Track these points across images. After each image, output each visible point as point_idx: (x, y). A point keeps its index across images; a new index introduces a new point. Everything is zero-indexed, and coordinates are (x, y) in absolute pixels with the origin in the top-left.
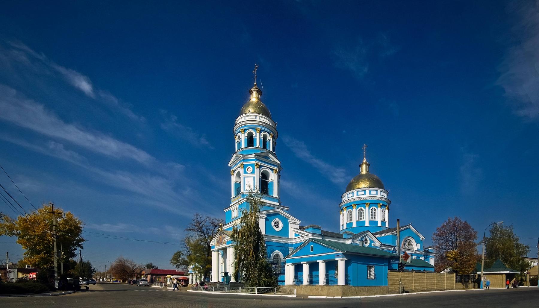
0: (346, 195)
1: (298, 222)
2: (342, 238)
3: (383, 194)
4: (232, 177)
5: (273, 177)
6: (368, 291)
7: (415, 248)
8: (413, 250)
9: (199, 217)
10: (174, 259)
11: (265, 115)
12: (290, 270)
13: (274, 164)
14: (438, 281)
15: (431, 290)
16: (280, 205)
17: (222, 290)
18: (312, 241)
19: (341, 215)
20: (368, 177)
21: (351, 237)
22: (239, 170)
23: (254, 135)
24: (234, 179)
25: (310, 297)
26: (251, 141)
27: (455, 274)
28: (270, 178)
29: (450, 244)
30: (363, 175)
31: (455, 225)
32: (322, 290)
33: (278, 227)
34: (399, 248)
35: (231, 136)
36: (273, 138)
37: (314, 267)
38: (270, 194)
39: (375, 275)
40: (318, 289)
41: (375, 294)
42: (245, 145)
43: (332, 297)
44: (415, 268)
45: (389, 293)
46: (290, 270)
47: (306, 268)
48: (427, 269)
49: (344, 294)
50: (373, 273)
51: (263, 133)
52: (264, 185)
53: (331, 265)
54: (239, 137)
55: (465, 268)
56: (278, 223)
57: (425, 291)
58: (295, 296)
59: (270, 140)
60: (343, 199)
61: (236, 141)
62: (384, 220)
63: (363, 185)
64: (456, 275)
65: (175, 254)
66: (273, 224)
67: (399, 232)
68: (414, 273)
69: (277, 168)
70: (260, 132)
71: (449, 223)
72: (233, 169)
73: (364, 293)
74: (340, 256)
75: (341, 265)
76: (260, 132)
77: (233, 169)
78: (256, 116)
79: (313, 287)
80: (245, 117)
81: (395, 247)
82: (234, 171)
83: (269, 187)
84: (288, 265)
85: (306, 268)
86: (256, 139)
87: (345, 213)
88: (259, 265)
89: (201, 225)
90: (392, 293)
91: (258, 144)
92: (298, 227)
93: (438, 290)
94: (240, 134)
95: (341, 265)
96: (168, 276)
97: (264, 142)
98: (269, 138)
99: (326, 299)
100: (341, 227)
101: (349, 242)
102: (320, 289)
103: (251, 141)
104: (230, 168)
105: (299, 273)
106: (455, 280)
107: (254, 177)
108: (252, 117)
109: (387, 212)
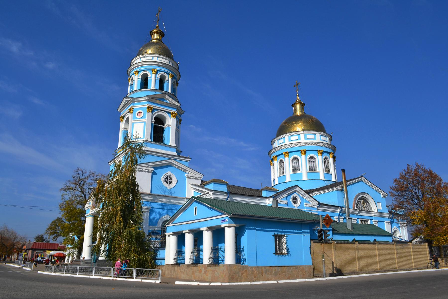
0: (276, 141)
1: (200, 176)
2: (261, 196)
3: (323, 138)
4: (121, 124)
5: (170, 122)
6: (276, 274)
7: (374, 209)
8: (371, 212)
9: (80, 172)
10: (50, 228)
11: (167, 56)
12: (171, 242)
13: (173, 106)
14: (400, 257)
15: (388, 271)
16: (179, 155)
17: (89, 271)
18: (196, 201)
19: (272, 167)
20: (303, 118)
21: (272, 194)
22: (129, 115)
23: (149, 76)
24: (122, 125)
25: (177, 283)
26: (144, 83)
27: (427, 245)
28: (167, 123)
29: (416, 201)
30: (297, 116)
31: (416, 175)
32: (205, 273)
33: (171, 183)
34: (349, 208)
35: (126, 77)
36: (173, 78)
37: (198, 237)
38: (166, 142)
39: (288, 249)
40: (201, 271)
41: (289, 278)
42: (137, 87)
43: (207, 284)
44: (358, 238)
45: (314, 277)
46: (171, 242)
47: (207, 237)
48: (379, 239)
49: (232, 279)
50: (284, 246)
51: (159, 74)
52: (158, 133)
53: (218, 234)
54: (133, 79)
55: (440, 235)
56: (171, 179)
57: (378, 272)
58: (158, 282)
59: (168, 81)
60: (276, 145)
61: (129, 84)
62: (329, 171)
63: (299, 127)
64: (430, 247)
65: (54, 222)
66: (163, 179)
67: (347, 186)
68: (356, 246)
69: (175, 111)
70: (156, 72)
71: (408, 172)
72: (123, 114)
73: (270, 276)
74: (227, 220)
75: (229, 234)
76: (156, 72)
77: (123, 114)
78: (153, 57)
79: (196, 268)
80: (141, 58)
81: (342, 207)
82: (124, 117)
83: (165, 133)
84: (169, 236)
85: (207, 237)
86: (151, 80)
87: (276, 163)
88: (132, 237)
89: (82, 183)
90: (320, 277)
91: (153, 83)
92: (199, 183)
93: (401, 270)
94: (133, 76)
95: (229, 234)
96: (47, 252)
97: (162, 82)
98: (167, 78)
99: (198, 287)
100: (272, 182)
101: (269, 202)
102: (203, 270)
103: (144, 83)
104: (120, 113)
105: (220, 245)
106: (428, 254)
107: (145, 122)
108: (148, 58)
109: (331, 160)
